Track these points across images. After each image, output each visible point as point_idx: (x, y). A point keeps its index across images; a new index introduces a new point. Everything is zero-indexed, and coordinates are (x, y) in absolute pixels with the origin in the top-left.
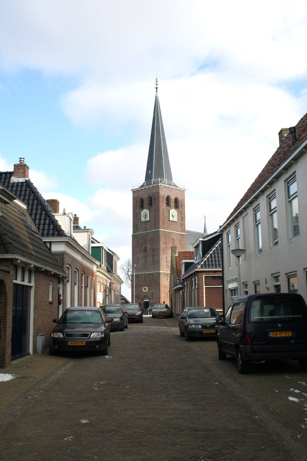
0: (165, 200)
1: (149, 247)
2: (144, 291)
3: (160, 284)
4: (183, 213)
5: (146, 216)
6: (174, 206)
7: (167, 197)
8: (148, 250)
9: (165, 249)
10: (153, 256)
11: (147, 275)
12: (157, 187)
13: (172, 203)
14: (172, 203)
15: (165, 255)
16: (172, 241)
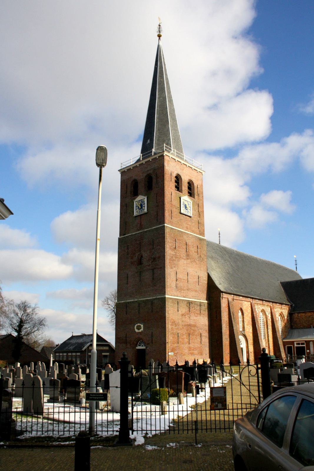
0: (174, 179)
1: (146, 255)
2: (137, 331)
3: (165, 317)
4: (200, 205)
5: (141, 205)
6: (187, 192)
7: (176, 177)
8: (145, 262)
9: (174, 258)
10: (153, 270)
11: (143, 304)
12: (160, 158)
13: (185, 187)
14: (185, 187)
15: (174, 269)
16: (185, 247)
